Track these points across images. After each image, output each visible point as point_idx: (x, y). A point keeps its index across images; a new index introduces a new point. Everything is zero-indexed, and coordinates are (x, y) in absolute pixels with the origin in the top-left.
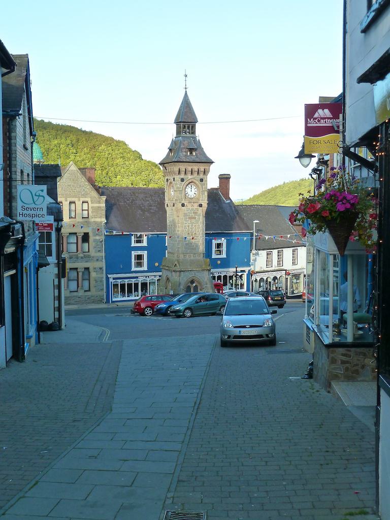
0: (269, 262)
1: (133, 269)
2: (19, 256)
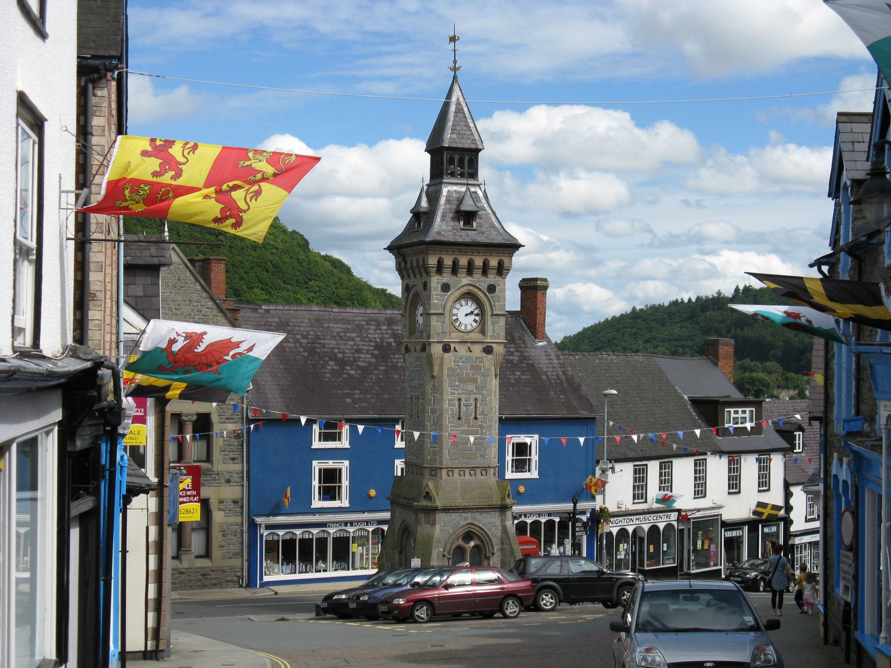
0: (640, 491)
2: (104, 460)
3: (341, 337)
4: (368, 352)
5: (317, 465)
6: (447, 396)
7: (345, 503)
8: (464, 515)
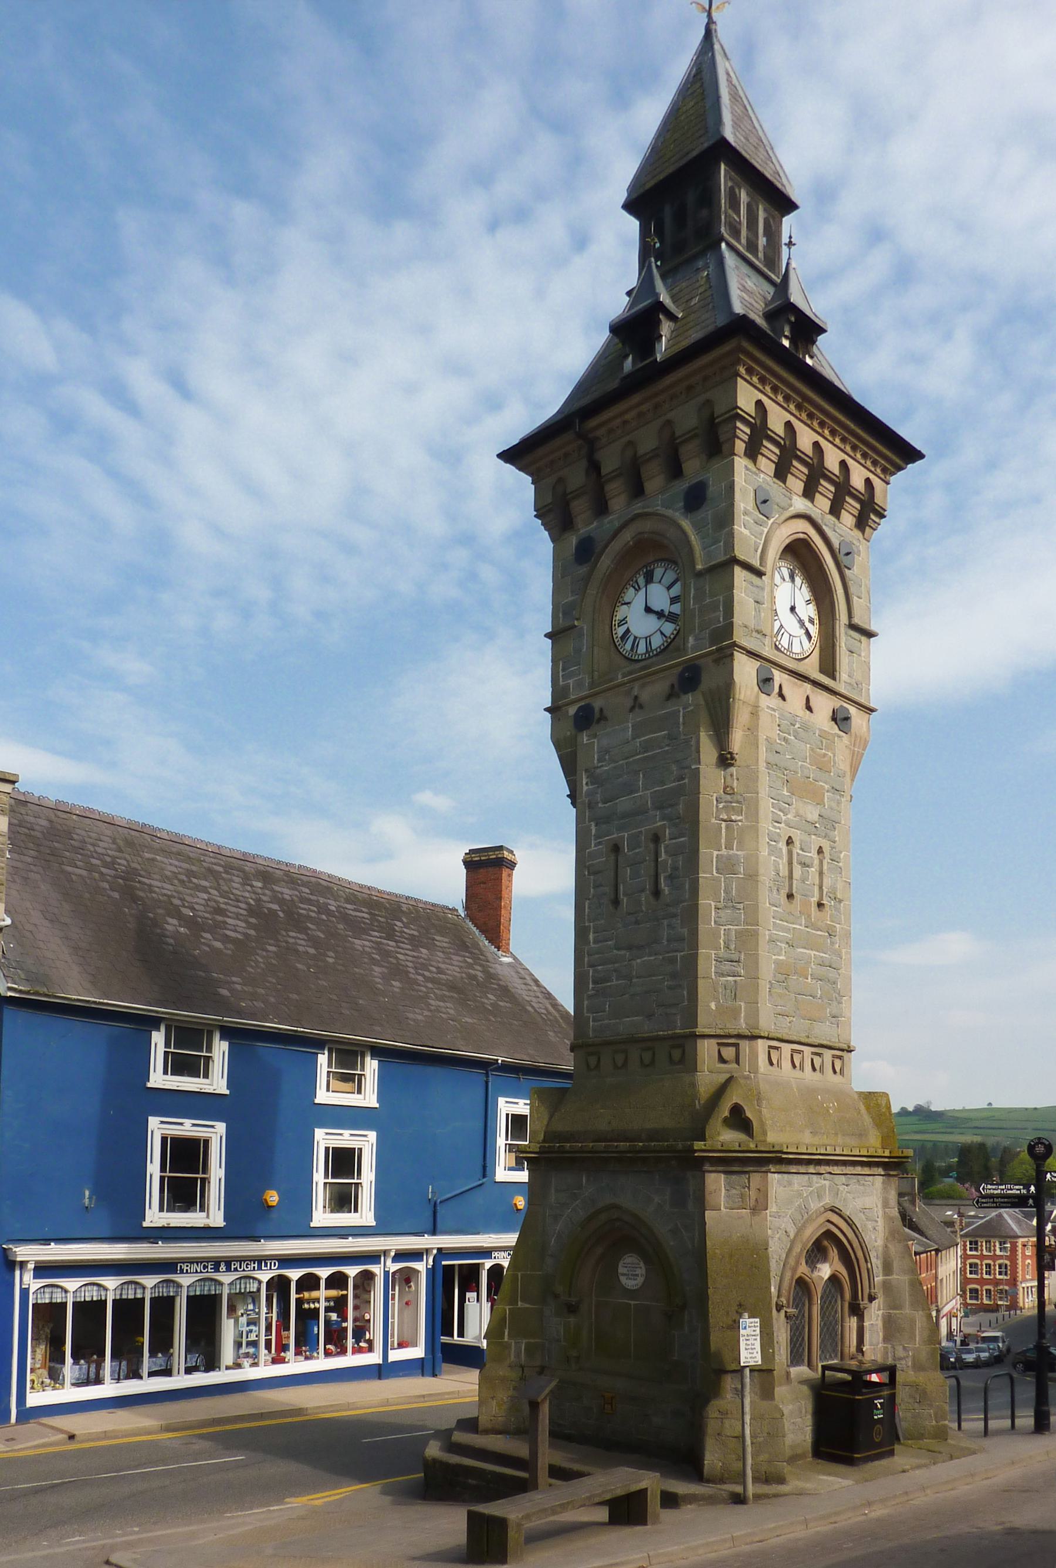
1: (155, 1217)
3: (182, 882)
4: (237, 916)
5: (157, 1127)
6: (766, 825)
7: (216, 1218)
8: (818, 1182)
